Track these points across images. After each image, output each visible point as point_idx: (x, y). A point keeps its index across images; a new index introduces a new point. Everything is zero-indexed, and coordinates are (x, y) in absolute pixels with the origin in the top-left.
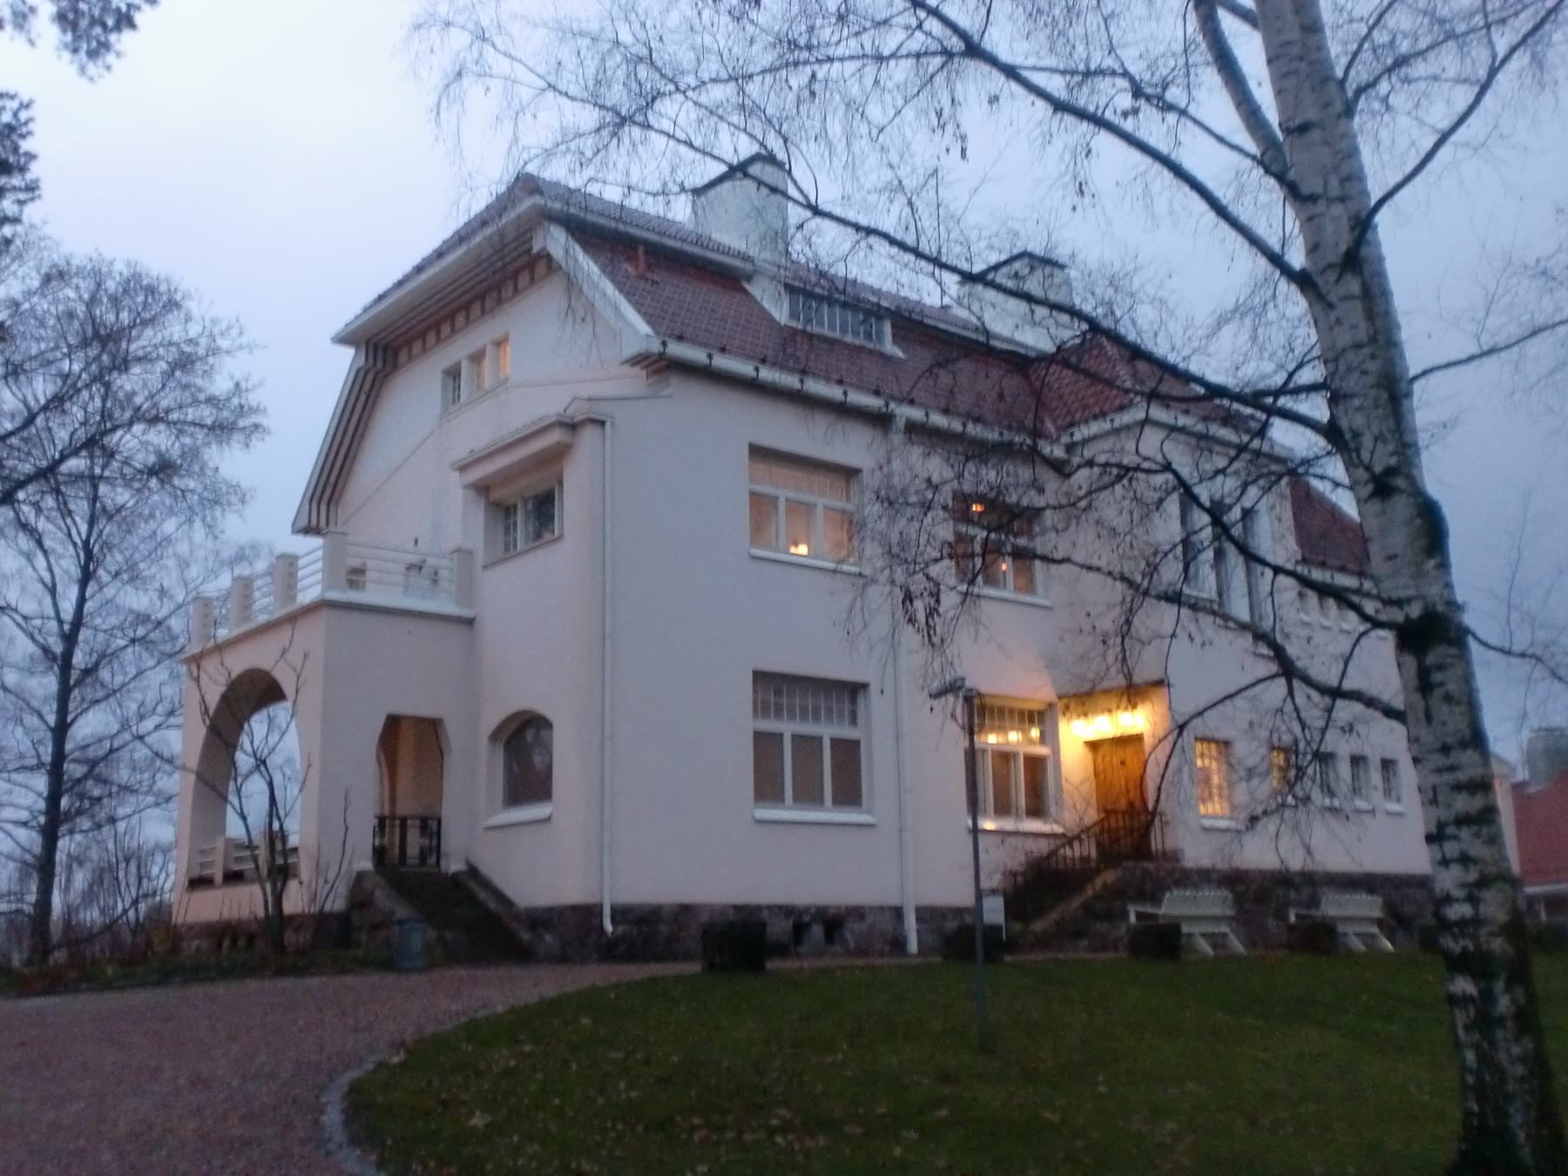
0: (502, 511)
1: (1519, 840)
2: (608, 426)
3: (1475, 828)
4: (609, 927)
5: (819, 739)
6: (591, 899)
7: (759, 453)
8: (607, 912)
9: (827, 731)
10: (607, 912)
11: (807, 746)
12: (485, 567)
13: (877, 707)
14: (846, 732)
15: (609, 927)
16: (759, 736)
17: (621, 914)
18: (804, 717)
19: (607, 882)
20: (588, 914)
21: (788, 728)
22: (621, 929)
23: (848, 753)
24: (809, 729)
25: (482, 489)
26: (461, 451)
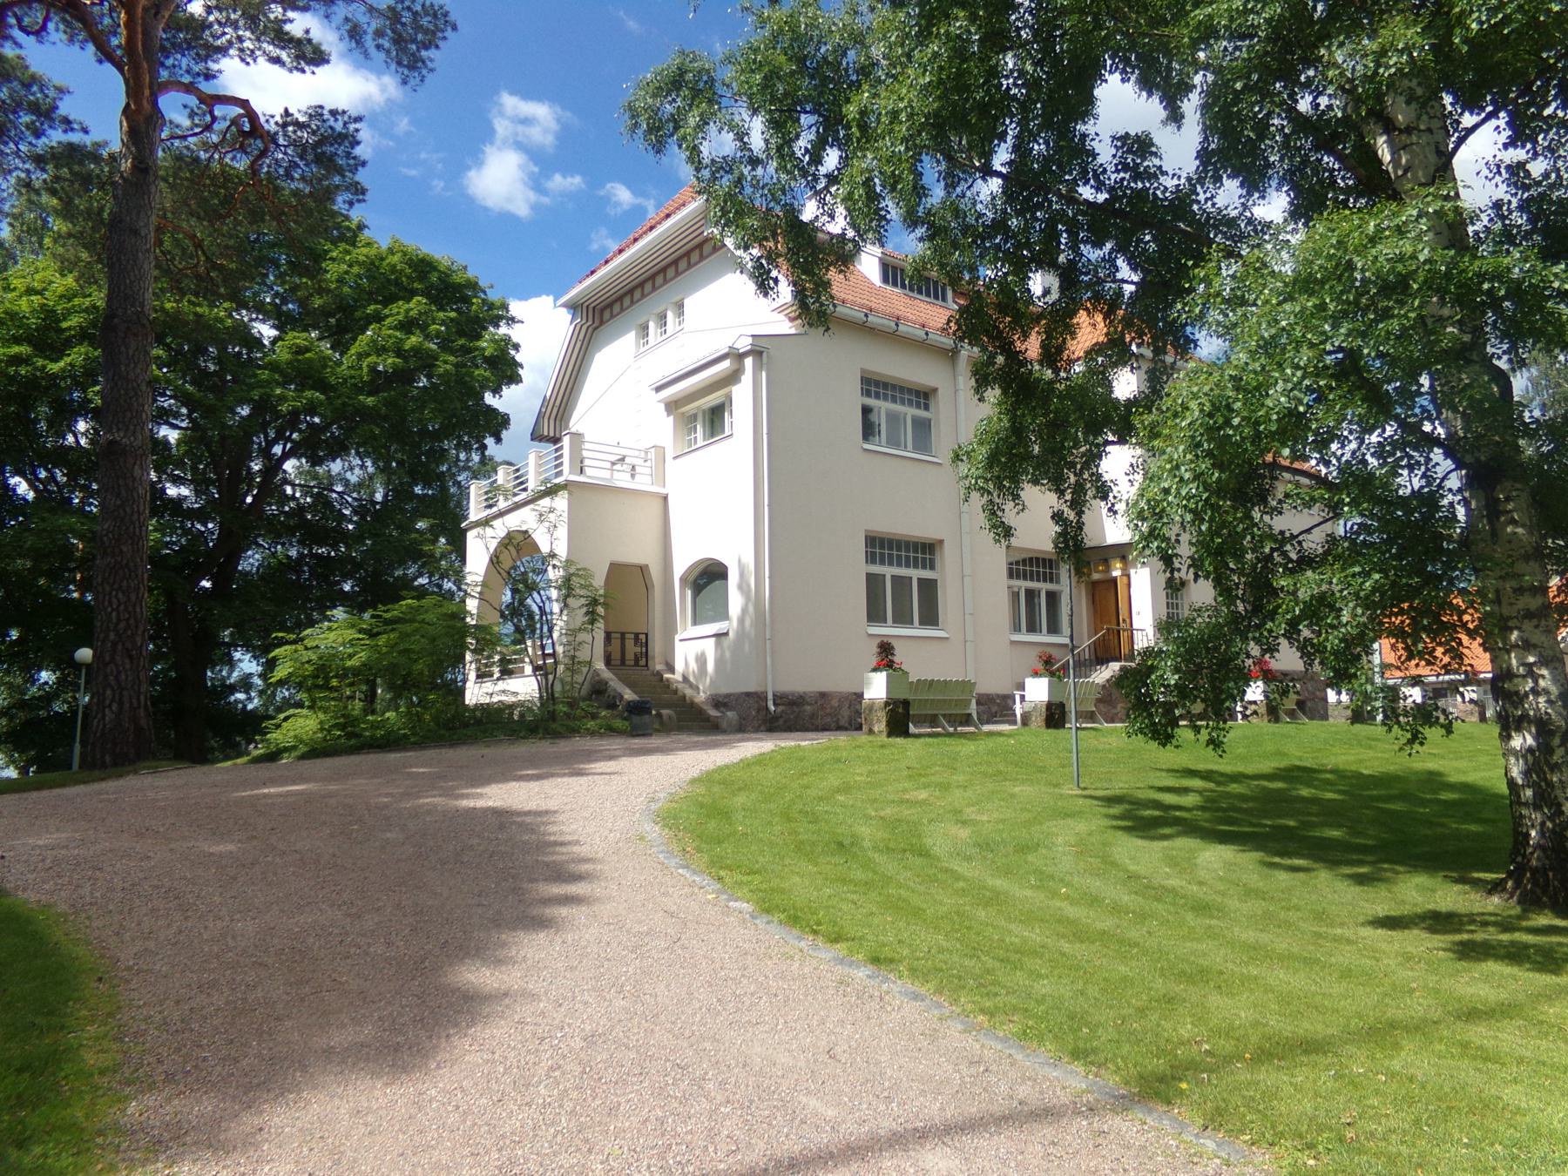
0: (686, 423)
1: (464, 743)
2: (765, 355)
3: (1535, 621)
4: (772, 708)
5: (921, 623)
6: (762, 689)
7: (873, 385)
8: (770, 696)
9: (915, 574)
10: (770, 696)
11: (901, 583)
12: (675, 458)
13: (948, 558)
14: (927, 574)
15: (772, 708)
16: (868, 575)
17: (779, 699)
18: (899, 565)
19: (770, 677)
20: (760, 697)
21: (889, 571)
22: (780, 708)
23: (928, 588)
24: (903, 571)
25: (672, 406)
26: (660, 376)
